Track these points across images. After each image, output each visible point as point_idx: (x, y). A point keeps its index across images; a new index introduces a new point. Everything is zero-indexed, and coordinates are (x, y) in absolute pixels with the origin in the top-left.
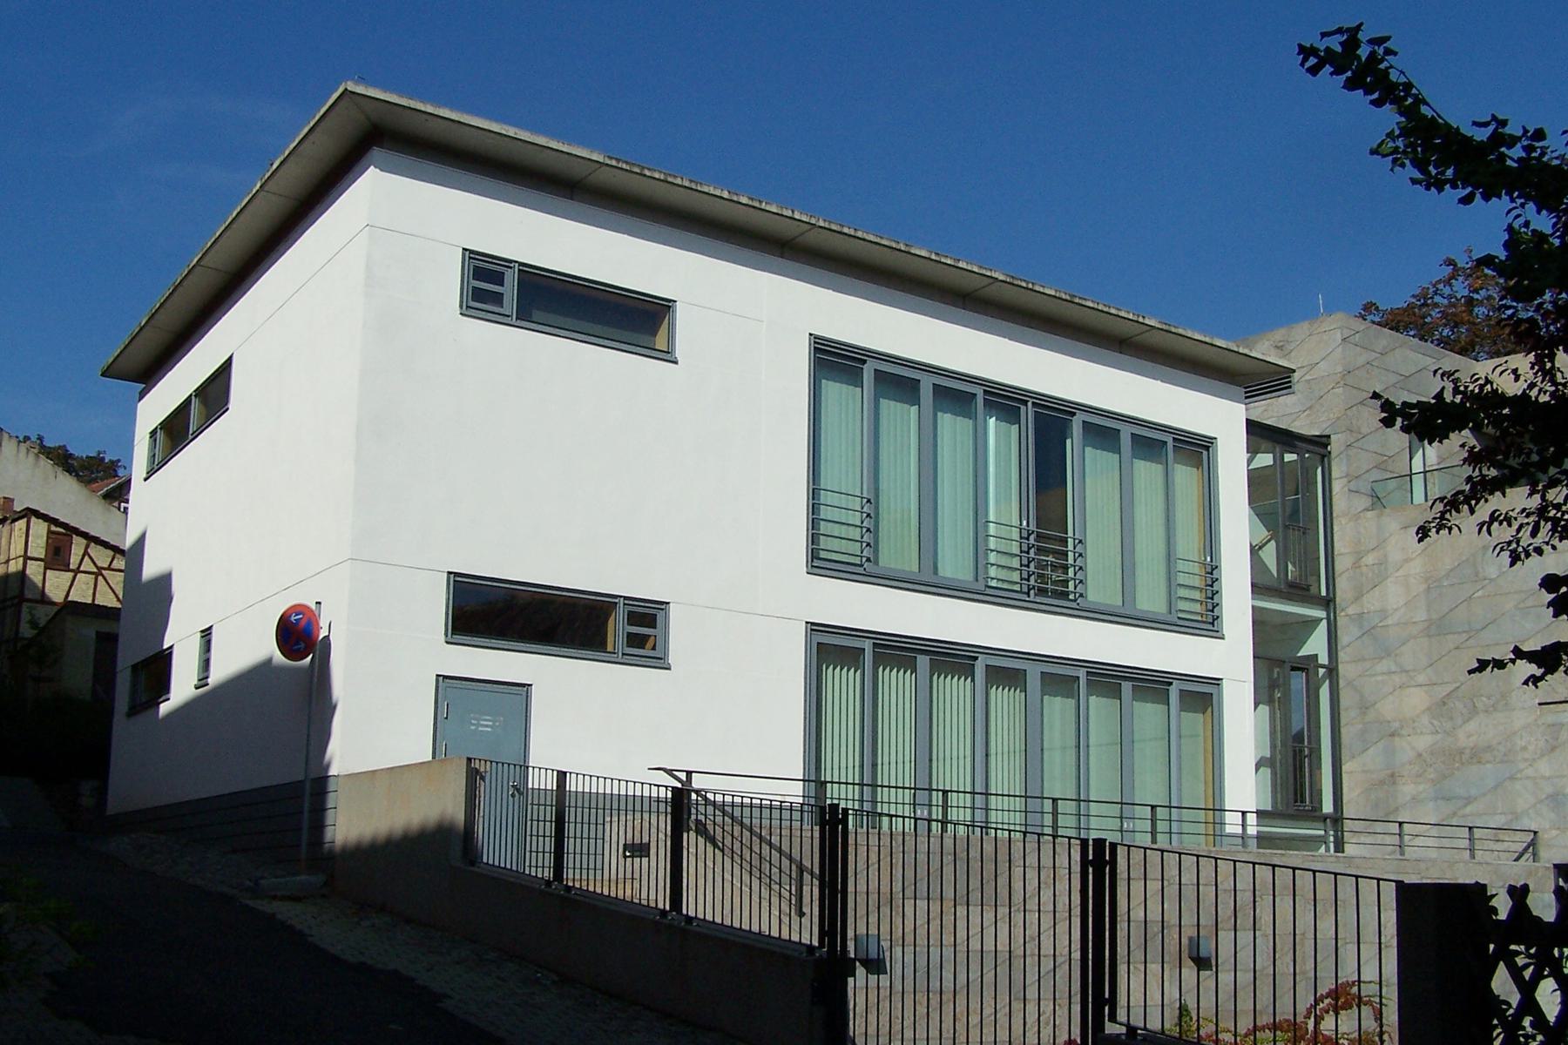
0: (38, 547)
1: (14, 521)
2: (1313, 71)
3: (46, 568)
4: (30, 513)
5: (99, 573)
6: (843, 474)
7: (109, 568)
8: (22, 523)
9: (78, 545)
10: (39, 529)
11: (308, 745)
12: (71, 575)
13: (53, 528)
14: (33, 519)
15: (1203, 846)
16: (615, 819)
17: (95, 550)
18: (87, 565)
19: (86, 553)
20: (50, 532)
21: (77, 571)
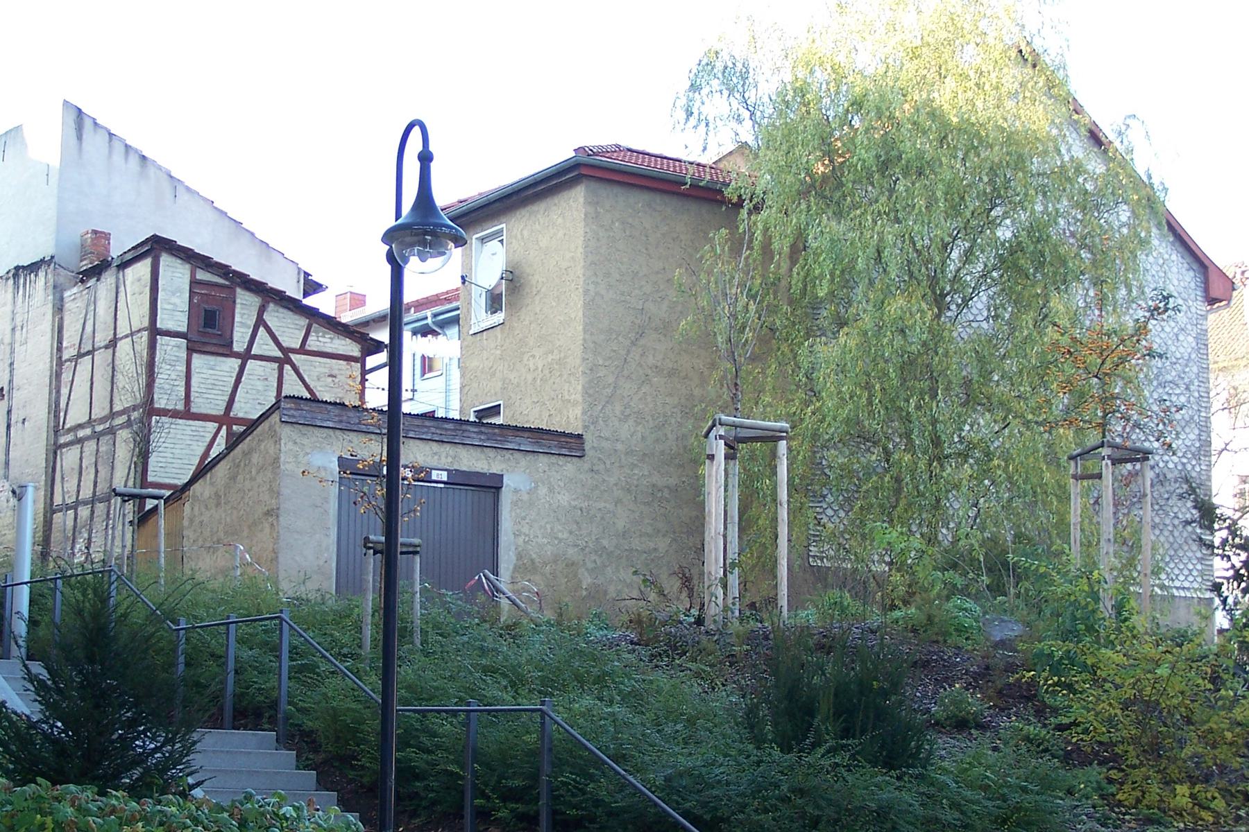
0: (174, 314)
1: (124, 265)
2: (52, 257)
3: (191, 350)
4: (156, 247)
5: (284, 359)
6: (213, 349)
7: (302, 350)
8: (142, 269)
9: (245, 307)
10: (175, 276)
11: (80, 481)
12: (235, 363)
13: (202, 275)
14: (166, 260)
15: (712, 612)
16: (351, 568)
17: (276, 317)
18: (264, 345)
19: (260, 322)
20: (194, 282)
21: (246, 356)
